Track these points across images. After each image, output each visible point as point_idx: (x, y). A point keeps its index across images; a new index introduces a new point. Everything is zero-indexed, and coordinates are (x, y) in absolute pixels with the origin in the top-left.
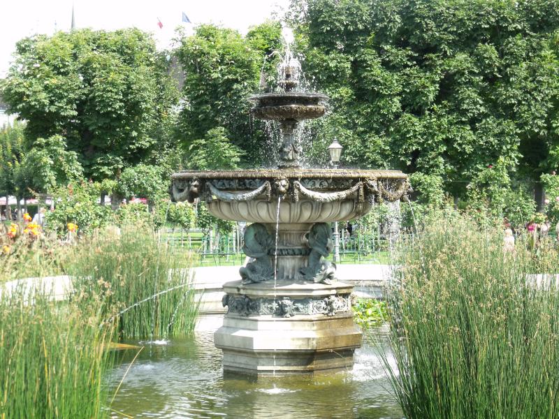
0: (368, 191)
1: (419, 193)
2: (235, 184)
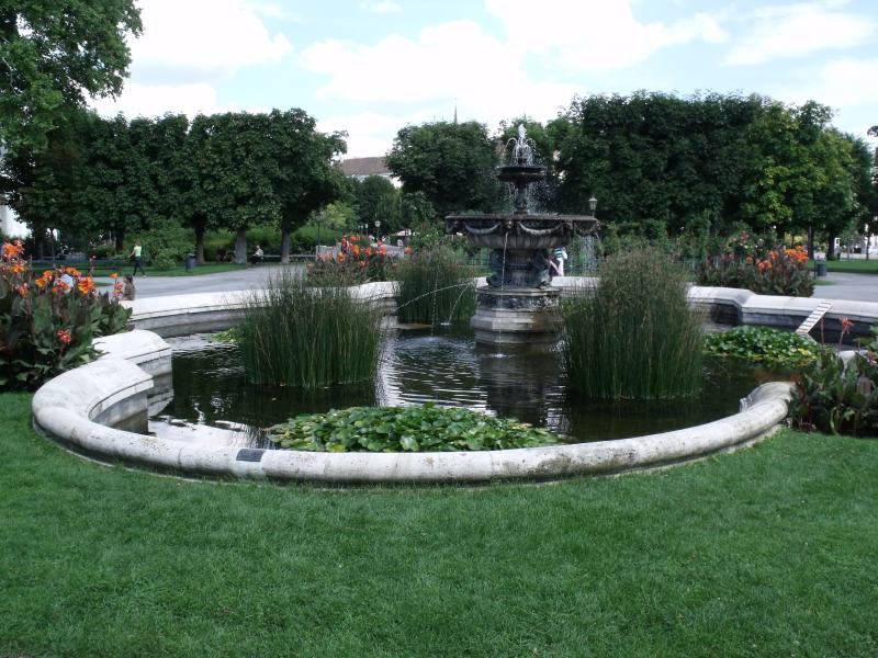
0: (566, 229)
1: (651, 232)
2: (480, 224)
